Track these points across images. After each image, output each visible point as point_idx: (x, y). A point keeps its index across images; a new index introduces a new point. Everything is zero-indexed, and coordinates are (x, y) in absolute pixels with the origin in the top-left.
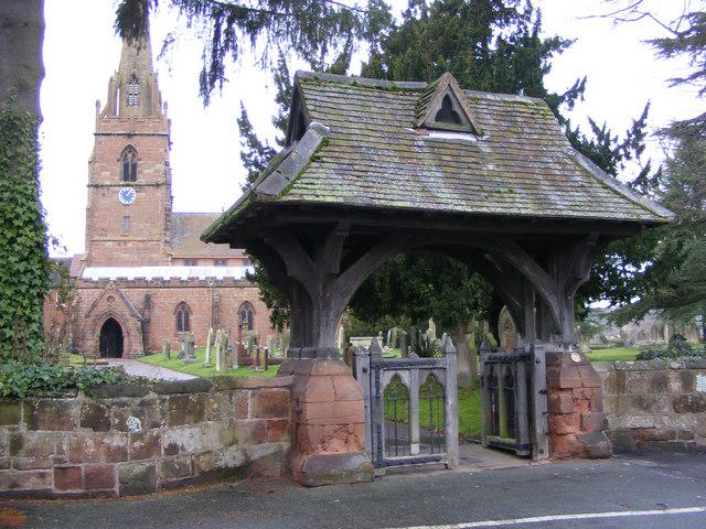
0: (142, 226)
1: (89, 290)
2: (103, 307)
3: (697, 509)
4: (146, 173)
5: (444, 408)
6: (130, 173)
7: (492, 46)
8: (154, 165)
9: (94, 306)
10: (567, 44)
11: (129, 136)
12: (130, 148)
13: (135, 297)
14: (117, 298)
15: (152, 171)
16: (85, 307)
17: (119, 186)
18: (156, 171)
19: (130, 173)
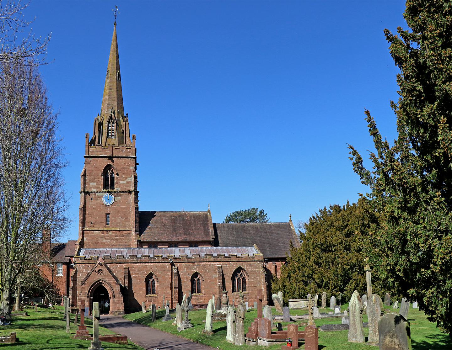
0: (118, 220)
1: (84, 265)
2: (95, 278)
3: (15, 323)
4: (123, 182)
5: (163, 243)
6: (108, 184)
7: (431, 249)
8: (126, 178)
9: (88, 276)
10: (399, 28)
11: (111, 158)
12: (109, 167)
13: (119, 270)
14: (105, 270)
15: (125, 182)
16: (81, 278)
17: (103, 192)
18: (128, 182)
19: (108, 184)
